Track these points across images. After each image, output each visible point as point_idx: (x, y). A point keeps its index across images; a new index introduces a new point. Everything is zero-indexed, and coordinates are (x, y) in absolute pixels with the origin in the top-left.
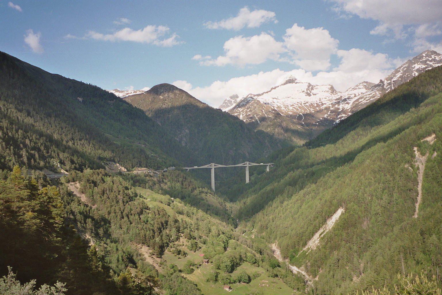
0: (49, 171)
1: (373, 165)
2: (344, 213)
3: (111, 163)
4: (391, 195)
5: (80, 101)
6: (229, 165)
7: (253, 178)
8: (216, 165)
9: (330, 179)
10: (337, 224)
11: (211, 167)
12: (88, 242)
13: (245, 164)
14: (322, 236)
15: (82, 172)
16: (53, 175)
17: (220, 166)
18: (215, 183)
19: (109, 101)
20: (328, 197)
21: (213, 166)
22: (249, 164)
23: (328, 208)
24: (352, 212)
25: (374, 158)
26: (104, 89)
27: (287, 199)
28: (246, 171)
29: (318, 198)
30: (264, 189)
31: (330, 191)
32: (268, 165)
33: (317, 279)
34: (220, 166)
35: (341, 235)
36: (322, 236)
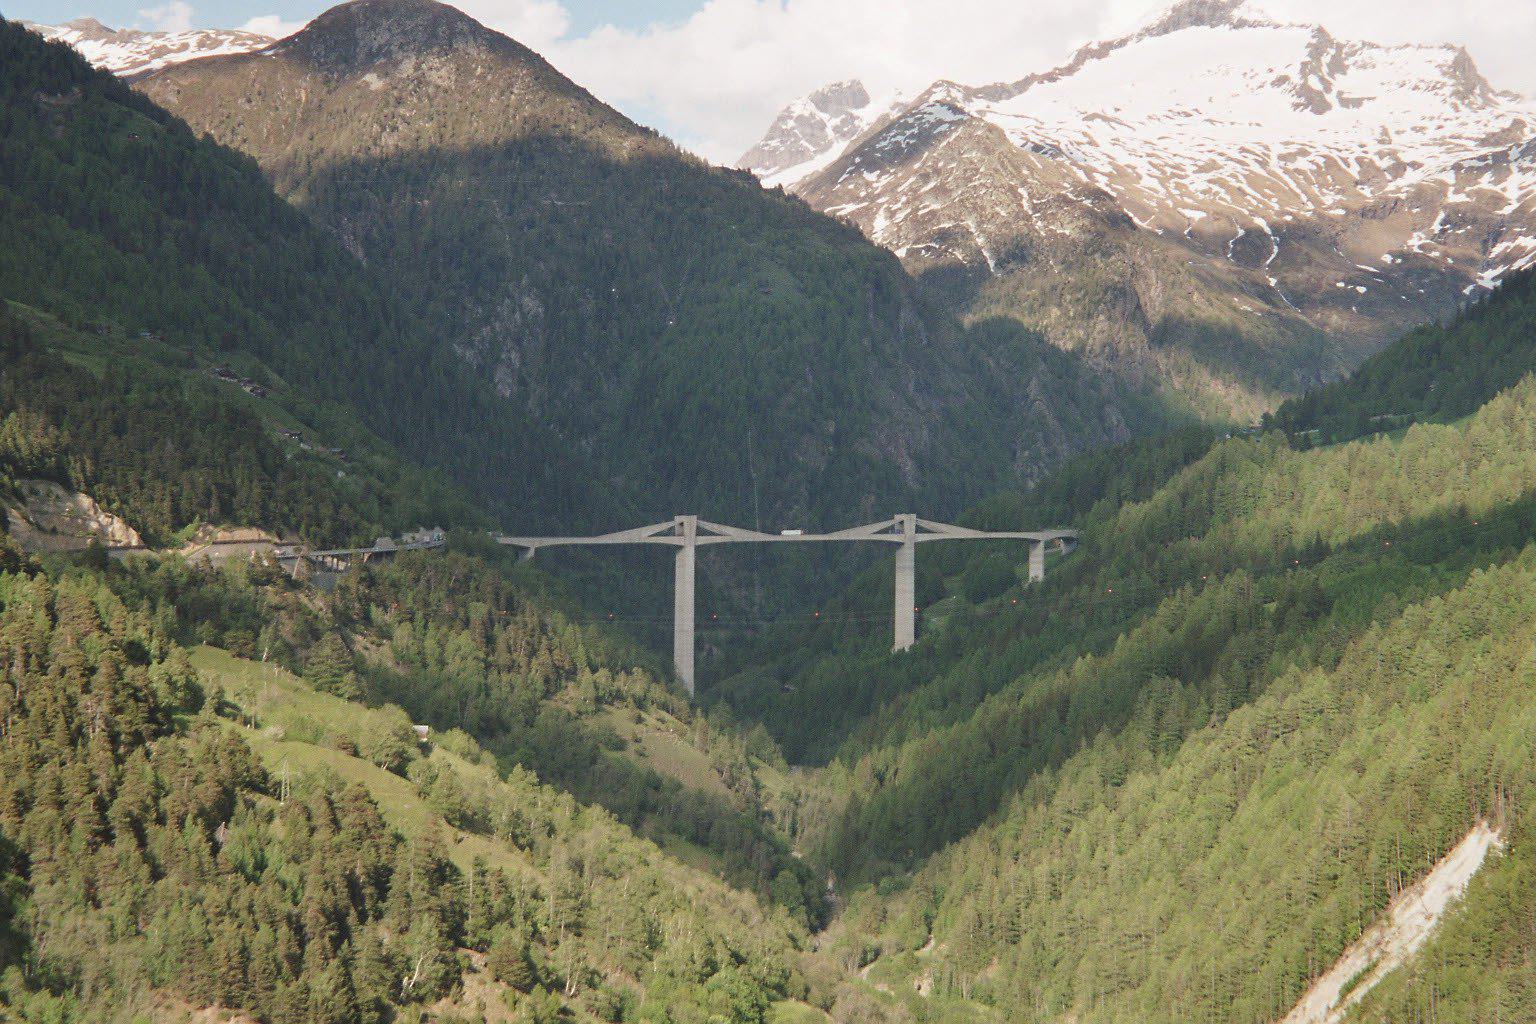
8: (708, 526)
12: (1026, 707)
13: (670, 532)
14: (1357, 996)
17: (734, 534)
22: (919, 530)
29: (1344, 755)
32: (1035, 542)
34: (734, 534)
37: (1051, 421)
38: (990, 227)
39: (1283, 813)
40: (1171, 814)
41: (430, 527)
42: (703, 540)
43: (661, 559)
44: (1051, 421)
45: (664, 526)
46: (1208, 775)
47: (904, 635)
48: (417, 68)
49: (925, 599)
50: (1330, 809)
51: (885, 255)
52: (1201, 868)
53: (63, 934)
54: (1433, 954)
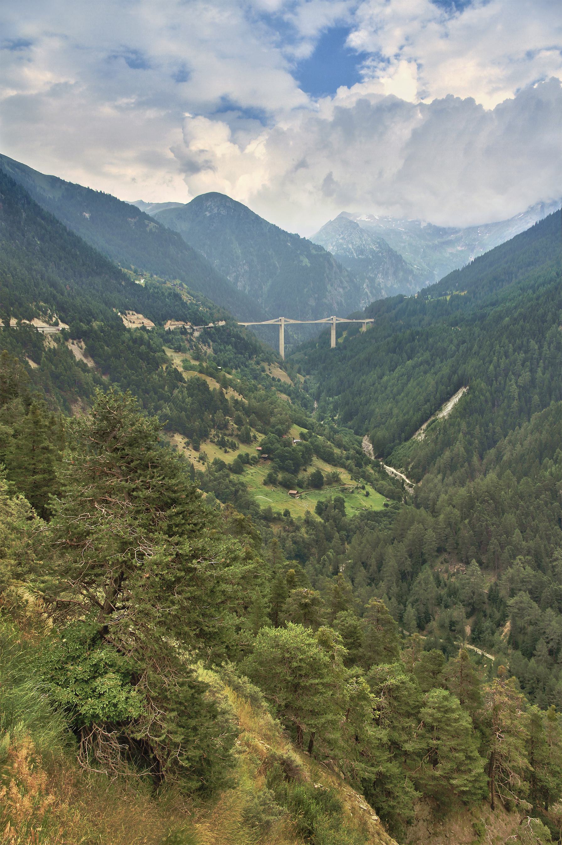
0: (41, 323)
1: (514, 325)
2: (466, 395)
3: (131, 312)
4: (533, 371)
5: (87, 218)
6: (308, 320)
7: (341, 340)
8: (287, 320)
9: (452, 345)
10: (455, 408)
11: (331, 322)
12: (121, 269)
13: (278, 321)
14: (432, 426)
15: (546, 321)
16: (48, 329)
17: (292, 321)
18: (285, 348)
19: (130, 219)
20: (446, 370)
21: (283, 321)
22: (337, 320)
23: (444, 387)
24: (477, 393)
25: (516, 315)
26: (121, 200)
27: (388, 372)
28: (332, 331)
29: (432, 371)
30: (357, 357)
31: (450, 362)
32: (364, 323)
33: (420, 484)
34: (292, 321)
35: (459, 425)
36: (432, 426)
37: (369, 294)
38: (354, 247)
39: (418, 384)
40: (393, 385)
41: (222, 321)
42: (286, 323)
43: (276, 328)
44: (369, 294)
45: (276, 320)
46: (402, 376)
47: (333, 344)
48: (218, 210)
49: (338, 336)
50: (428, 384)
51: (329, 254)
52: (400, 397)
53: (400, 704)
54: (450, 415)
